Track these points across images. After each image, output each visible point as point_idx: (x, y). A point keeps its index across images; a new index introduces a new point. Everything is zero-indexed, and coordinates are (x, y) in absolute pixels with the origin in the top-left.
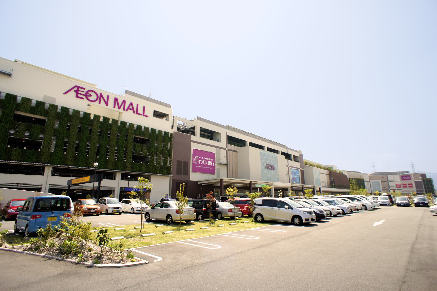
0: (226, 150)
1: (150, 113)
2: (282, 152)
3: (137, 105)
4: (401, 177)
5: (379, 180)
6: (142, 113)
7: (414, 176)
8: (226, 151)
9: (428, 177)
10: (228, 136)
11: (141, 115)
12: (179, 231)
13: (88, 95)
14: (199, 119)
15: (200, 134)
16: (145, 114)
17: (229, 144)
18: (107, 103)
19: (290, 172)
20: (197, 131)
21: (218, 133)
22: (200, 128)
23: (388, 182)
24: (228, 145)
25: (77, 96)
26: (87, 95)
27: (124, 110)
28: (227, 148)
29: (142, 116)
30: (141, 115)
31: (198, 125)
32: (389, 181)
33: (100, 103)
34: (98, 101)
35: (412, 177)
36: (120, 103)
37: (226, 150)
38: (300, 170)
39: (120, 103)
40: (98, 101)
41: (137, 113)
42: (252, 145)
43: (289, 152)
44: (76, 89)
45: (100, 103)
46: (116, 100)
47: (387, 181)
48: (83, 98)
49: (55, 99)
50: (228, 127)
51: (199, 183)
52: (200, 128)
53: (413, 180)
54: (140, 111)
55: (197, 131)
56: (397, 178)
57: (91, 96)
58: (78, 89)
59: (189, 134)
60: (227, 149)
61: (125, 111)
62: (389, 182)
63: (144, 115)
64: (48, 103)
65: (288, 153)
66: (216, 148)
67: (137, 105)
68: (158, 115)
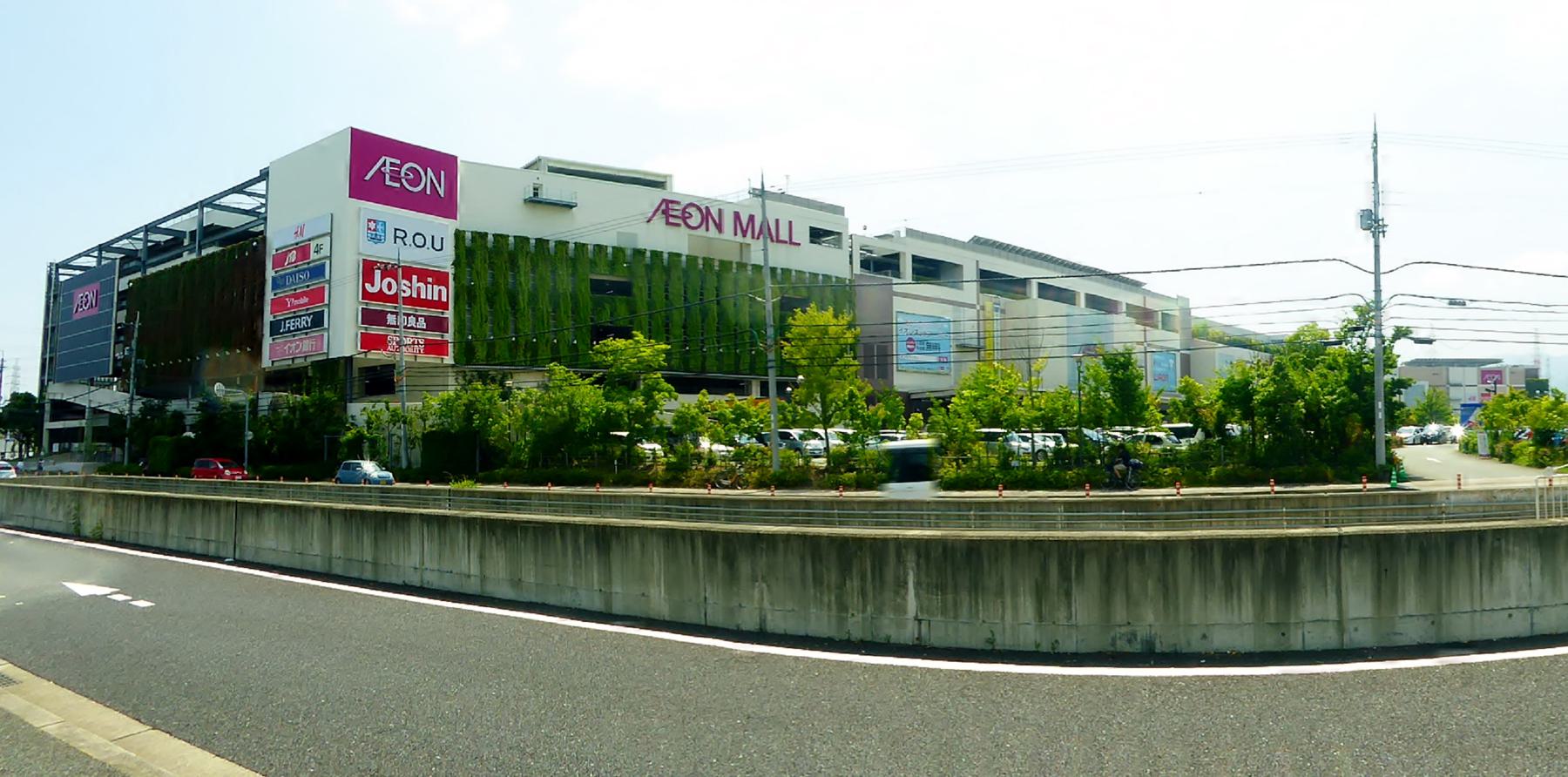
0: (975, 308)
1: (802, 235)
2: (915, 259)
3: (777, 221)
4: (1480, 373)
5: (1425, 380)
6: (787, 239)
7: (1512, 373)
8: (975, 311)
9: (1543, 376)
10: (981, 270)
11: (786, 242)
12: (476, 482)
13: (687, 215)
14: (910, 232)
15: (913, 269)
16: (793, 241)
17: (982, 292)
18: (719, 227)
19: (1148, 361)
20: (907, 267)
21: (956, 265)
22: (913, 256)
23: (1448, 388)
24: (981, 295)
25: (668, 223)
26: (685, 216)
27: (753, 237)
28: (978, 303)
29: (788, 245)
30: (786, 242)
31: (909, 250)
32: (1452, 385)
33: (707, 229)
34: (704, 226)
35: (1507, 377)
36: (745, 220)
37: (975, 308)
38: (1178, 354)
39: (745, 220)
40: (704, 226)
41: (779, 241)
42: (1046, 291)
43: (1151, 304)
44: (663, 207)
45: (707, 229)
46: (737, 216)
47: (1444, 386)
48: (678, 225)
49: (635, 236)
50: (979, 243)
51: (913, 397)
52: (913, 256)
53: (1508, 383)
54: (784, 235)
55: (907, 267)
56: (1472, 375)
57: (691, 216)
58: (667, 206)
59: (887, 275)
60: (978, 307)
61: (755, 240)
62: (1451, 388)
63: (791, 243)
64: (627, 245)
65: (1147, 307)
66: (951, 306)
67: (777, 221)
68: (817, 235)
